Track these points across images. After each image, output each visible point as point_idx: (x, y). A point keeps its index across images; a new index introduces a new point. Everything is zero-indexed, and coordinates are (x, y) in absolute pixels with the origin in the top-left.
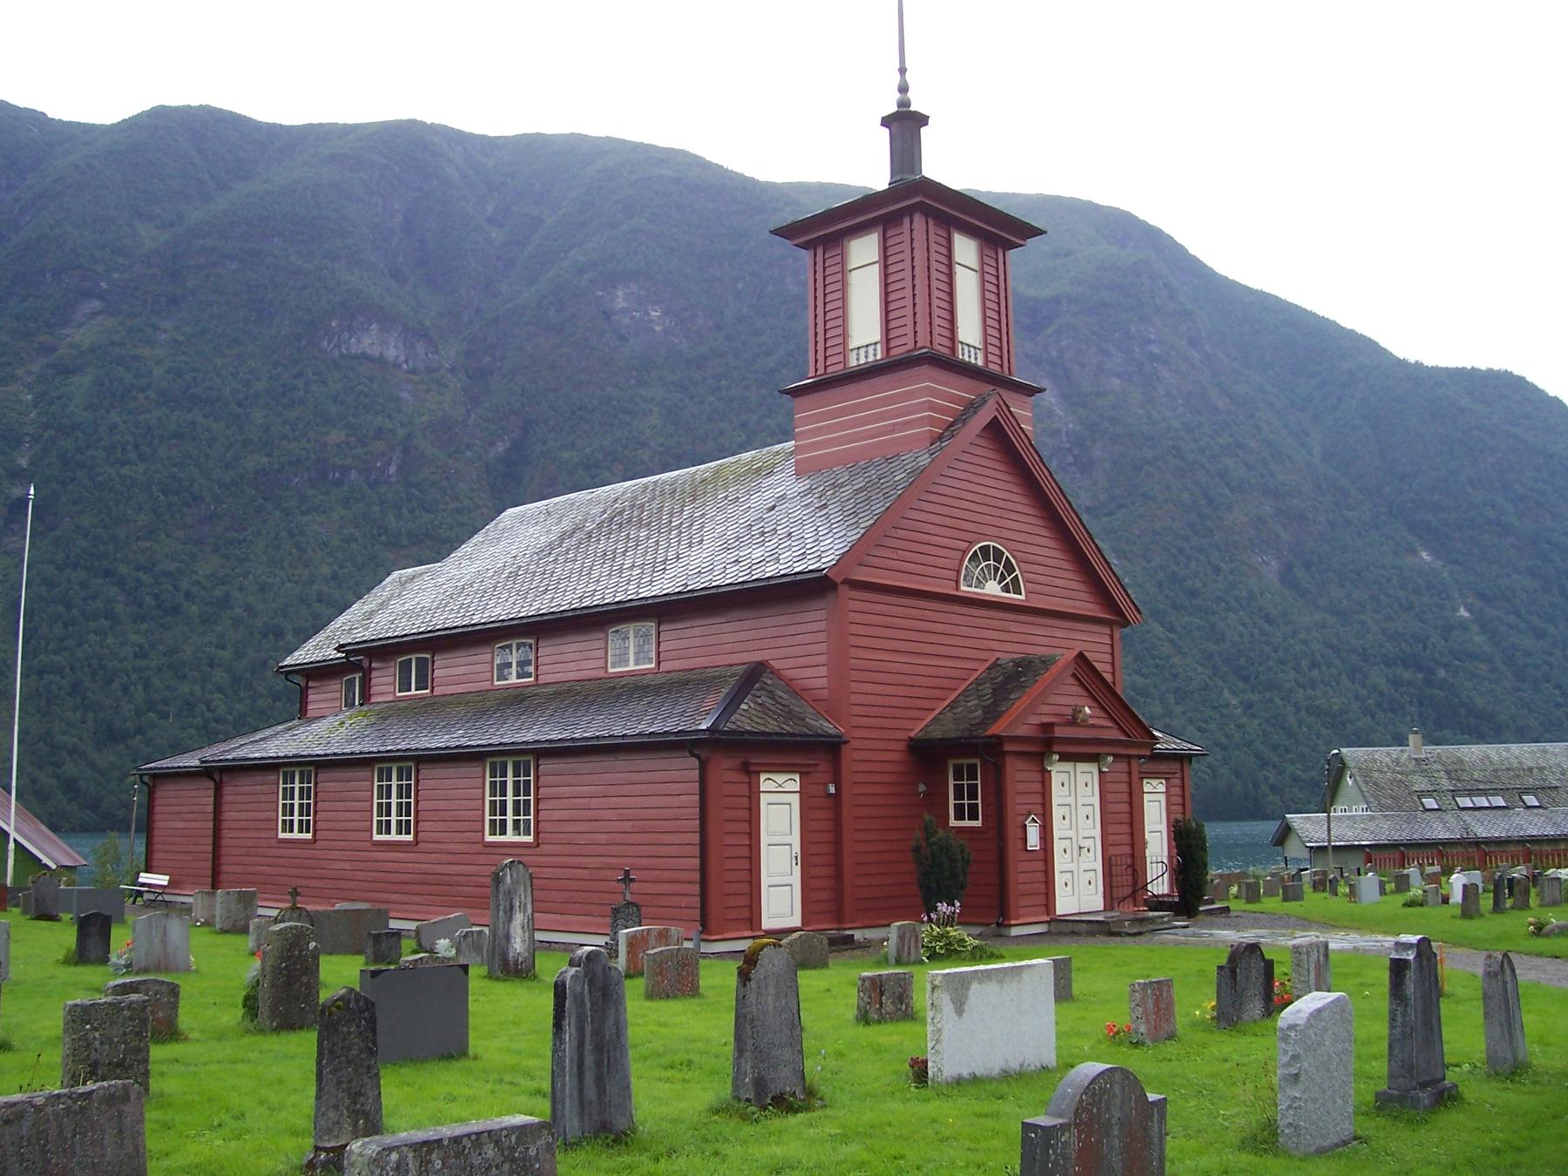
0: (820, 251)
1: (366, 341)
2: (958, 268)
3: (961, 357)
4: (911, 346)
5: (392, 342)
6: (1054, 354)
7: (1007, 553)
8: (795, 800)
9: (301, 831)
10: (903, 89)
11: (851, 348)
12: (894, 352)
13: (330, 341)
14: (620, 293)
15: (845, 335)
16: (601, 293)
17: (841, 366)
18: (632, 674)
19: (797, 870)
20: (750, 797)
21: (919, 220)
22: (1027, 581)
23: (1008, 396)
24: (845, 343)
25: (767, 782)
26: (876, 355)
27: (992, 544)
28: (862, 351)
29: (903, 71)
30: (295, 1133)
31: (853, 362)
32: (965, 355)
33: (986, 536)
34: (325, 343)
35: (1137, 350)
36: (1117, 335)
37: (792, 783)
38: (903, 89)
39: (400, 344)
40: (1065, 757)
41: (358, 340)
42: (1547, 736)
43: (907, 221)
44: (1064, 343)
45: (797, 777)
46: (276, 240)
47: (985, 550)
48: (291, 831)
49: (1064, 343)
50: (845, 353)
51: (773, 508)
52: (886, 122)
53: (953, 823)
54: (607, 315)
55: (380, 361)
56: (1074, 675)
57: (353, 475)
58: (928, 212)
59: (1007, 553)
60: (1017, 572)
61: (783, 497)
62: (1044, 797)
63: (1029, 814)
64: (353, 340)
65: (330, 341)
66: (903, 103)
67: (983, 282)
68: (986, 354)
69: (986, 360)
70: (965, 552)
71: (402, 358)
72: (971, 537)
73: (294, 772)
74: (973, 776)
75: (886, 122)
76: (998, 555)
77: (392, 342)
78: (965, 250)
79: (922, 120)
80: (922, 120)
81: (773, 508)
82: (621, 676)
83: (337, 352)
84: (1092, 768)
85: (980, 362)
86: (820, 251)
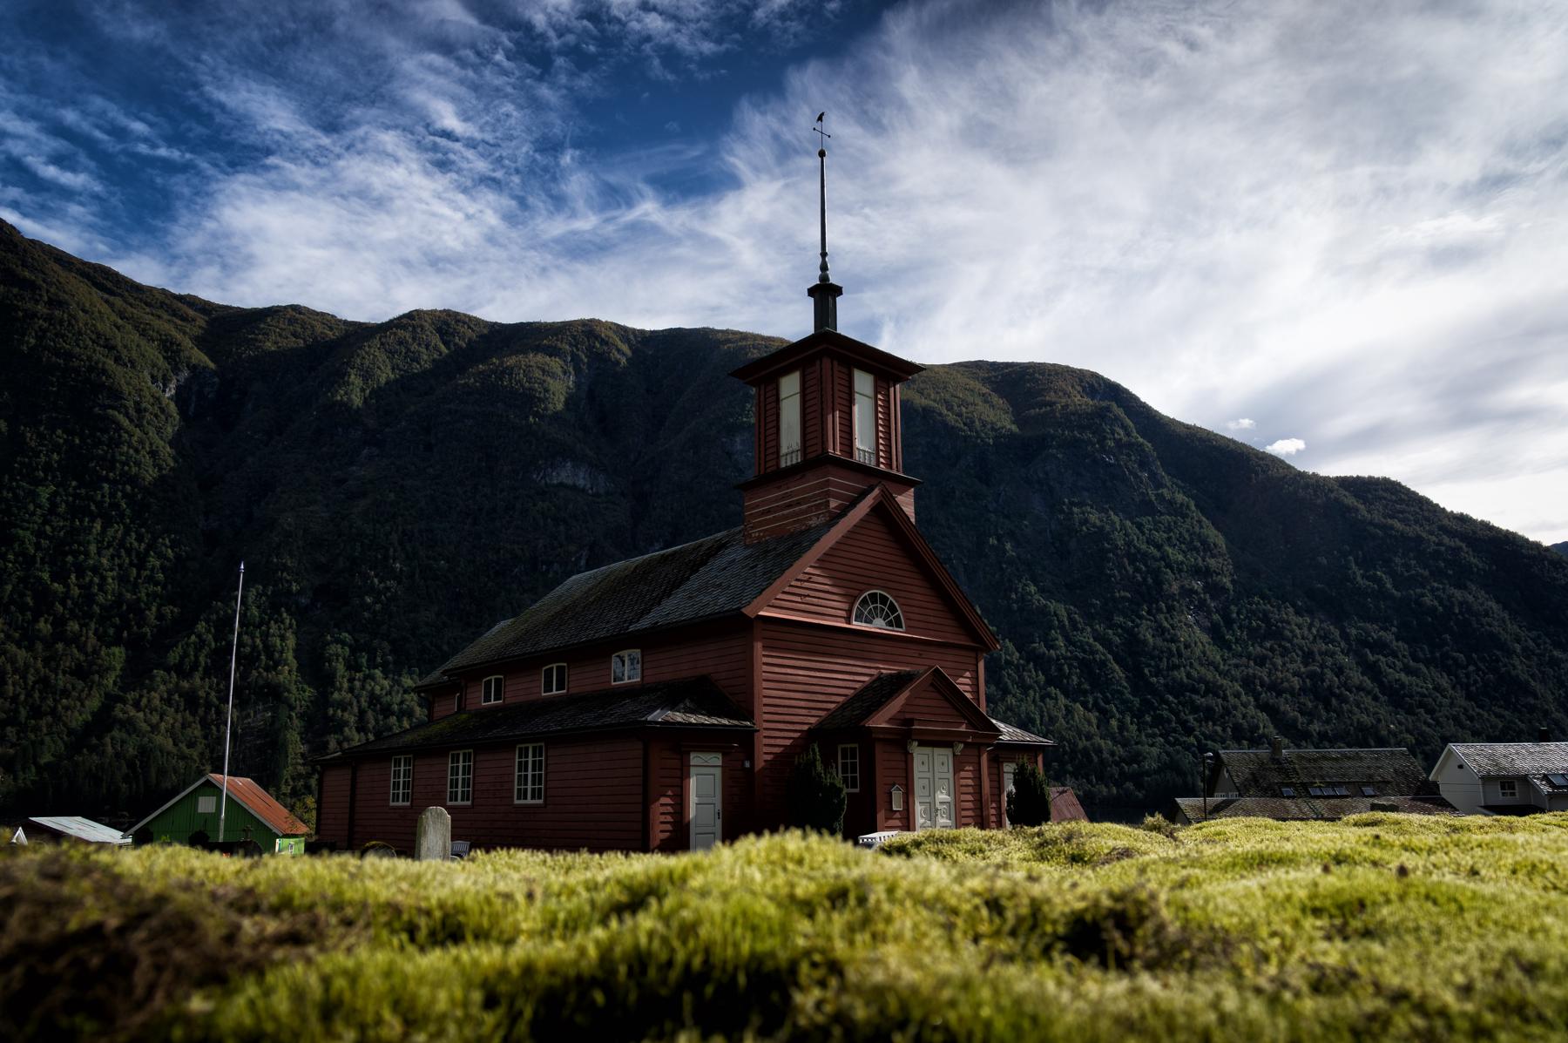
1: (563, 474)
2: (857, 396)
3: (831, 450)
4: (820, 452)
5: (581, 475)
6: (1041, 475)
8: (718, 772)
9: (463, 800)
10: (824, 267)
14: (738, 439)
15: (778, 446)
17: (775, 468)
18: (626, 685)
19: (719, 823)
20: (682, 770)
21: (827, 362)
22: (907, 619)
25: (695, 759)
26: (796, 459)
27: (878, 592)
28: (789, 457)
29: (824, 254)
30: (1421, 984)
31: (783, 465)
32: (858, 457)
34: (535, 476)
37: (716, 759)
38: (824, 267)
39: (587, 476)
40: (922, 744)
43: (818, 363)
45: (720, 756)
46: (499, 404)
47: (873, 596)
48: (526, 798)
51: (725, 569)
53: (543, 744)
55: (574, 488)
56: (932, 685)
59: (891, 598)
60: (900, 612)
62: (907, 773)
63: (894, 785)
66: (824, 278)
71: (589, 486)
73: (459, 754)
74: (854, 757)
76: (884, 600)
77: (581, 475)
78: (863, 383)
79: (838, 291)
80: (838, 291)
81: (725, 569)
82: (619, 687)
83: (543, 481)
84: (948, 752)
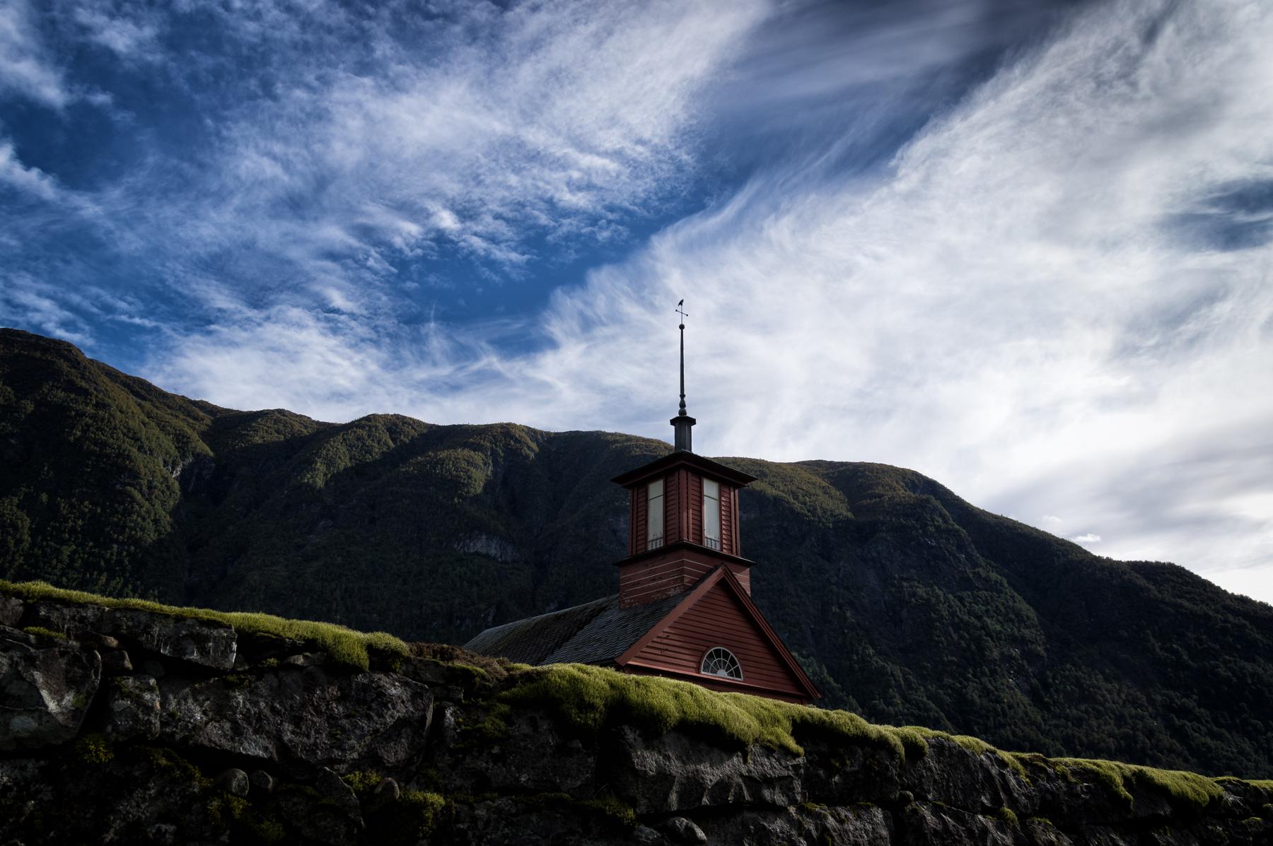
0: (636, 490)
2: (705, 498)
7: (731, 654)
10: (683, 405)
11: (718, 548)
12: (669, 543)
13: (458, 545)
15: (646, 534)
16: (611, 520)
21: (683, 473)
22: (745, 671)
23: (731, 566)
24: (646, 538)
29: (682, 396)
31: (650, 549)
32: (707, 544)
33: (717, 644)
35: (925, 552)
36: (912, 543)
38: (683, 405)
41: (474, 544)
42: (1083, 754)
43: (677, 474)
44: (880, 548)
47: (717, 652)
49: (880, 548)
50: (646, 542)
52: (673, 422)
54: (615, 532)
55: (487, 556)
57: (468, 621)
58: (688, 469)
59: (731, 654)
61: (610, 621)
64: (472, 544)
65: (458, 545)
66: (682, 412)
67: (720, 505)
68: (722, 544)
69: (722, 549)
70: (704, 653)
71: (499, 555)
72: (707, 644)
75: (673, 422)
76: (726, 655)
79: (693, 422)
80: (693, 422)
85: (718, 548)
86: (636, 490)
